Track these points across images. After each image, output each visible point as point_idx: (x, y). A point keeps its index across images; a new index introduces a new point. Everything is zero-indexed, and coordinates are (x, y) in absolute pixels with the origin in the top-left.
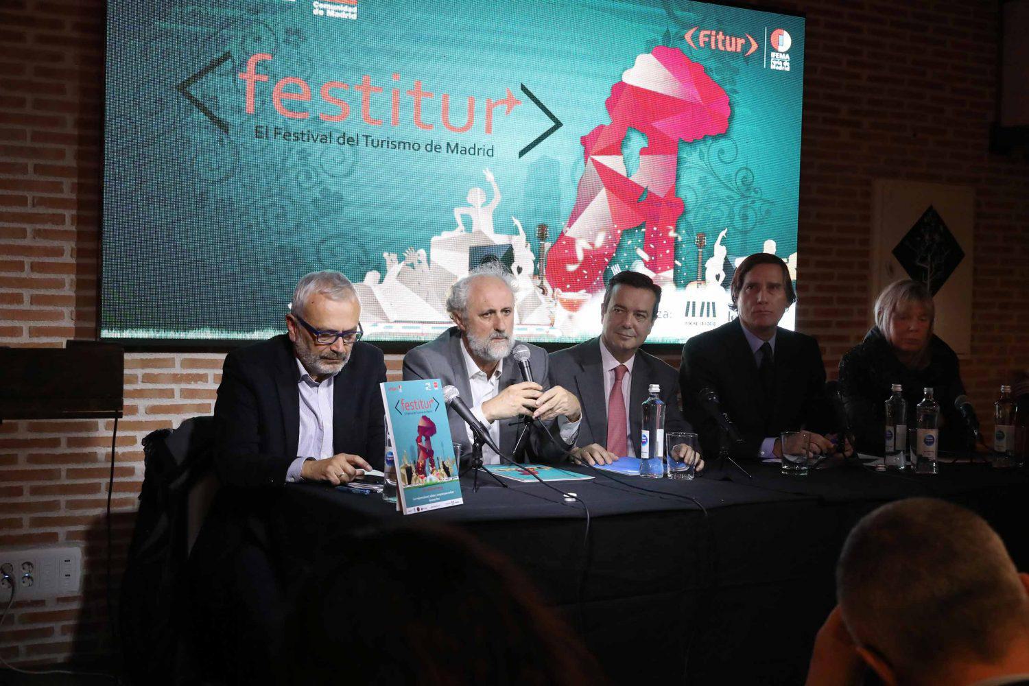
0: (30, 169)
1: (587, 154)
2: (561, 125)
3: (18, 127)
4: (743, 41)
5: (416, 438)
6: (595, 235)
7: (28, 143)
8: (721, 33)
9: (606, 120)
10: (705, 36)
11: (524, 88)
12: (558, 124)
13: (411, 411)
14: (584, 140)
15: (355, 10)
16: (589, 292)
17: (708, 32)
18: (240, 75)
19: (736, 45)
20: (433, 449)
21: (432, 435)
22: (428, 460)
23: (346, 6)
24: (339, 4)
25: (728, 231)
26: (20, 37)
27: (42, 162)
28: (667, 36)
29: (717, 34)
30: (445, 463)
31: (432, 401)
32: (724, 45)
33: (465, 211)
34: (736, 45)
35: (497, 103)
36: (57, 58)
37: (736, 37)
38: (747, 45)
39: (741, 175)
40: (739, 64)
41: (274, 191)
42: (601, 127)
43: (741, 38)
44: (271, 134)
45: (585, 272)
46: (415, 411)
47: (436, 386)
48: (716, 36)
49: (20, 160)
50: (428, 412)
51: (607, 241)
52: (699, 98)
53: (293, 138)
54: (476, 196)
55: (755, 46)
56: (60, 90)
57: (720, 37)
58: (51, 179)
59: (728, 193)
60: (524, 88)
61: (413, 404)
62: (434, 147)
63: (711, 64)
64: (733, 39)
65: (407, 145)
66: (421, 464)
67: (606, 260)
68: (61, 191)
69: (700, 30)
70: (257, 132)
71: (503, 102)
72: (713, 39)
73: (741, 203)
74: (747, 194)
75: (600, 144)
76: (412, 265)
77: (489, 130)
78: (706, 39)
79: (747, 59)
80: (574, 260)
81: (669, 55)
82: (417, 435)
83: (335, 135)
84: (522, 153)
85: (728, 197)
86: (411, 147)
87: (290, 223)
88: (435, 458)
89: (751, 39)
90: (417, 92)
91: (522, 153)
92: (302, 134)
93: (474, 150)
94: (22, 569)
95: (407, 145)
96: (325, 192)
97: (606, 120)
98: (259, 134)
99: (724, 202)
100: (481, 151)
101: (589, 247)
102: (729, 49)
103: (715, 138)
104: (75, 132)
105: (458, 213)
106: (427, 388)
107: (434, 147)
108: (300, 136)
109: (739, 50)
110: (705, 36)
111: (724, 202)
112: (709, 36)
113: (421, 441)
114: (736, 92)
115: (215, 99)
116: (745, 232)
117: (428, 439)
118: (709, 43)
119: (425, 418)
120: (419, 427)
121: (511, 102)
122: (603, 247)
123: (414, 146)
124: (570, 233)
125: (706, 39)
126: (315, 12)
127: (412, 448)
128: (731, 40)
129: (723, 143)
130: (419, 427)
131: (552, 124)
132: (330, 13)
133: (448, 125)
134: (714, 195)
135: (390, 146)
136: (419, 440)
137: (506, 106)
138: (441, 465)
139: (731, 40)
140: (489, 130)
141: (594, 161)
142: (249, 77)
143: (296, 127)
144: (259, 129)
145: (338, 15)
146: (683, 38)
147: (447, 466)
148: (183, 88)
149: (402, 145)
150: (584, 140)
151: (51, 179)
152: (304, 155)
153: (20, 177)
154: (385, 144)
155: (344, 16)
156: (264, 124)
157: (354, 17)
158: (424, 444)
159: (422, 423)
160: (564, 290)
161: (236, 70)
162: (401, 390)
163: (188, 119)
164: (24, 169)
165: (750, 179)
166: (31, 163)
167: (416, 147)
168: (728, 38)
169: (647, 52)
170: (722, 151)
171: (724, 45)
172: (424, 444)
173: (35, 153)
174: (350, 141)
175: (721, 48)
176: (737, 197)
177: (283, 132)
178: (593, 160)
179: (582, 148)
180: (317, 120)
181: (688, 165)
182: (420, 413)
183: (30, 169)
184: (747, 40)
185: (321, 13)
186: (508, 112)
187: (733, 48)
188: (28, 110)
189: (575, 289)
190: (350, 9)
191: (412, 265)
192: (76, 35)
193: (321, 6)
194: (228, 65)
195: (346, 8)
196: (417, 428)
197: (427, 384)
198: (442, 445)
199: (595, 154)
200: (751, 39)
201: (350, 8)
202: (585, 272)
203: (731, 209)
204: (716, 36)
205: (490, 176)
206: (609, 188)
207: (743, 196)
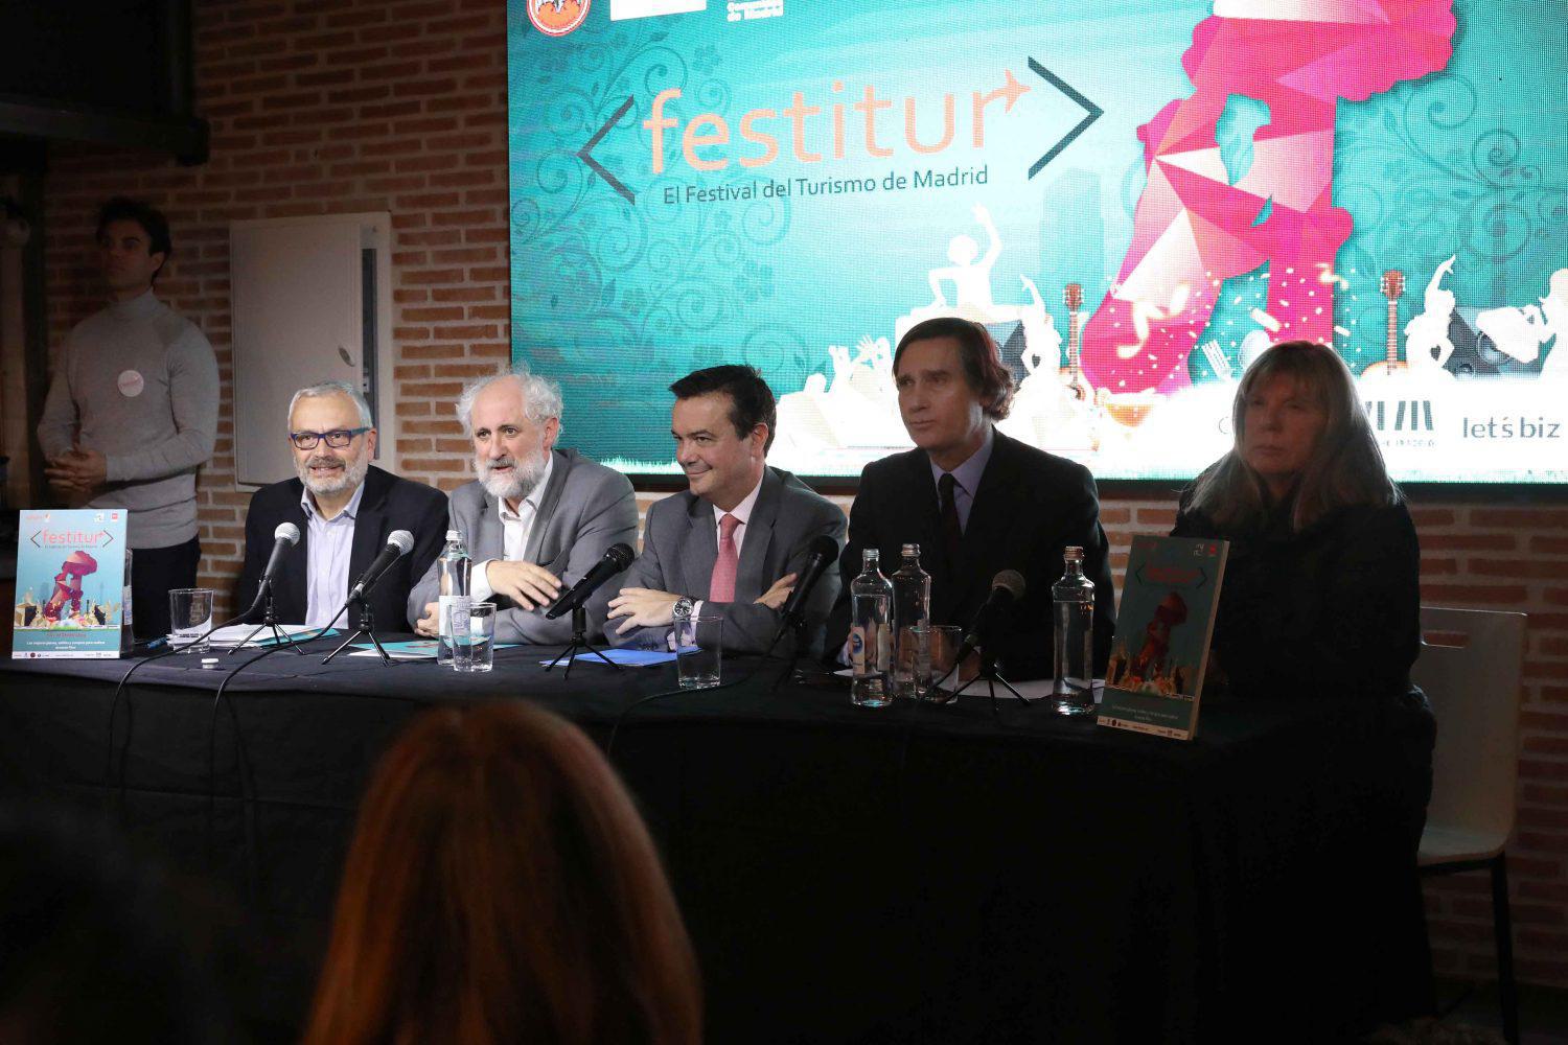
0: (467, 275)
1: (1149, 155)
7: (464, 245)
11: (1033, 64)
12: (1095, 112)
14: (1143, 133)
42: (1175, 105)
44: (683, 194)
53: (708, 197)
60: (1033, 64)
65: (857, 185)
73: (1491, 202)
84: (1033, 172)
86: (863, 186)
88: (83, 600)
91: (1033, 172)
103: (1420, 83)
108: (717, 194)
117: (77, 578)
127: (45, 587)
129: (1437, 91)
132: (747, 16)
135: (834, 189)
138: (92, 609)
149: (850, 185)
150: (1143, 133)
153: (457, 285)
154: (826, 187)
159: (72, 558)
162: (47, 520)
164: (459, 276)
166: (466, 267)
173: (469, 255)
177: (696, 191)
178: (1161, 164)
181: (1359, 143)
183: (467, 275)
186: (1008, 108)
188: (462, 207)
203: (1466, 218)
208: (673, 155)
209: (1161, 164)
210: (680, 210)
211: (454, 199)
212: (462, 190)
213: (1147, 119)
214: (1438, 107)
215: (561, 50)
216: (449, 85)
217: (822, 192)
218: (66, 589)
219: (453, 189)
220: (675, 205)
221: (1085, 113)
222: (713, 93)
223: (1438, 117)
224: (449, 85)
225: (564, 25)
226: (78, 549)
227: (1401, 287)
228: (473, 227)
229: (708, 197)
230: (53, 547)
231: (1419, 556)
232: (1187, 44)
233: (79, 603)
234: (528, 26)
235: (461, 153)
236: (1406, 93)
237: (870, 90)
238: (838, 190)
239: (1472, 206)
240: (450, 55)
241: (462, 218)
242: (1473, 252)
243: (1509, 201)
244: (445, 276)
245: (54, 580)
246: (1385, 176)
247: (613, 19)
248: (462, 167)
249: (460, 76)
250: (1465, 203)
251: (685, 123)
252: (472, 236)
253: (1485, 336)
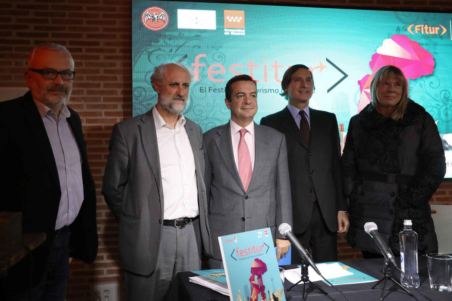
0: (103, 114)
1: (361, 89)
2: (348, 76)
3: (98, 96)
4: (438, 28)
5: (249, 278)
7: (102, 103)
8: (426, 26)
10: (418, 28)
11: (327, 60)
12: (346, 76)
13: (245, 257)
14: (359, 82)
15: (244, 31)
17: (420, 26)
19: (435, 31)
20: (264, 284)
21: (263, 273)
22: (260, 295)
23: (240, 30)
24: (236, 29)
25: (438, 121)
26: (98, 58)
27: (108, 110)
28: (398, 29)
29: (424, 26)
30: (275, 294)
31: (263, 246)
32: (429, 31)
34: (435, 31)
36: (113, 65)
37: (435, 27)
38: (441, 30)
39: (444, 92)
40: (438, 41)
41: (143, 103)
42: (368, 76)
43: (437, 27)
44: (207, 89)
46: (249, 255)
47: (266, 234)
48: (424, 28)
49: (99, 110)
50: (259, 255)
52: (418, 59)
53: (217, 91)
55: (445, 30)
56: (115, 78)
57: (426, 27)
58: (112, 118)
59: (436, 103)
60: (327, 60)
61: (247, 251)
63: (422, 41)
64: (433, 28)
65: (272, 91)
66: (254, 299)
69: (415, 24)
70: (201, 89)
71: (317, 67)
72: (422, 29)
73: (444, 107)
74: (447, 103)
78: (419, 29)
79: (441, 37)
81: (401, 40)
82: (251, 275)
84: (329, 91)
85: (437, 105)
86: (274, 91)
88: (266, 291)
89: (442, 27)
91: (329, 91)
92: (222, 89)
94: (105, 293)
95: (272, 91)
98: (202, 91)
99: (434, 107)
102: (431, 33)
103: (427, 76)
104: (122, 96)
106: (259, 237)
108: (221, 90)
109: (437, 33)
110: (418, 28)
111: (434, 107)
112: (420, 28)
113: (254, 280)
114: (436, 53)
116: (447, 122)
117: (260, 277)
118: (420, 31)
119: (257, 260)
120: (252, 269)
125: (419, 29)
126: (226, 33)
127: (246, 287)
128: (432, 29)
129: (431, 79)
130: (252, 269)
131: (343, 76)
132: (232, 34)
134: (429, 105)
135: (264, 91)
136: (252, 279)
137: (319, 69)
138: (272, 297)
139: (432, 29)
144: (202, 88)
145: (236, 34)
146: (406, 30)
147: (277, 296)
149: (270, 90)
150: (359, 82)
151: (112, 118)
153: (99, 118)
154: (262, 91)
155: (239, 34)
156: (204, 86)
157: (244, 34)
158: (256, 282)
159: (255, 265)
162: (236, 241)
164: (100, 114)
165: (448, 95)
166: (103, 111)
167: (277, 91)
168: (430, 28)
169: (388, 38)
170: (431, 83)
171: (429, 31)
172: (256, 282)
173: (104, 106)
175: (427, 33)
176: (441, 104)
177: (213, 89)
178: (364, 91)
179: (359, 86)
181: (414, 90)
182: (253, 257)
183: (103, 114)
184: (441, 28)
185: (228, 34)
186: (320, 72)
187: (433, 32)
188: (102, 88)
190: (242, 31)
192: (121, 54)
193: (228, 30)
195: (240, 30)
196: (250, 270)
197: (258, 233)
198: (272, 280)
199: (365, 89)
200: (442, 27)
201: (242, 30)
203: (439, 110)
204: (424, 28)
206: (255, 287)
207: (445, 104)
208: (203, 76)
209: (364, 91)
210: (206, 95)
211: (98, 85)
212: (102, 83)
213: (360, 79)
214: (431, 83)
215: (157, 36)
216: (97, 44)
217: (260, 92)
218: (256, 286)
219: (97, 82)
220: (205, 93)
221: (343, 76)
222: (219, 57)
223: (432, 85)
224: (97, 44)
225: (159, 27)
226: (256, 258)
227: (343, 128)
228: (106, 96)
229: (217, 91)
230: (243, 259)
231: (96, 205)
232: (370, 60)
233: (265, 294)
234: (141, 25)
235: (102, 69)
236: (424, 78)
237: (276, 62)
238: (266, 92)
239: (440, 108)
240: (97, 33)
241: (102, 92)
242: (441, 120)
243: (448, 107)
244: (93, 114)
245: (249, 282)
246: (421, 99)
247: (178, 28)
248: (101, 74)
249: (102, 41)
250: (439, 107)
251: (208, 66)
252: (105, 100)
253: (445, 141)
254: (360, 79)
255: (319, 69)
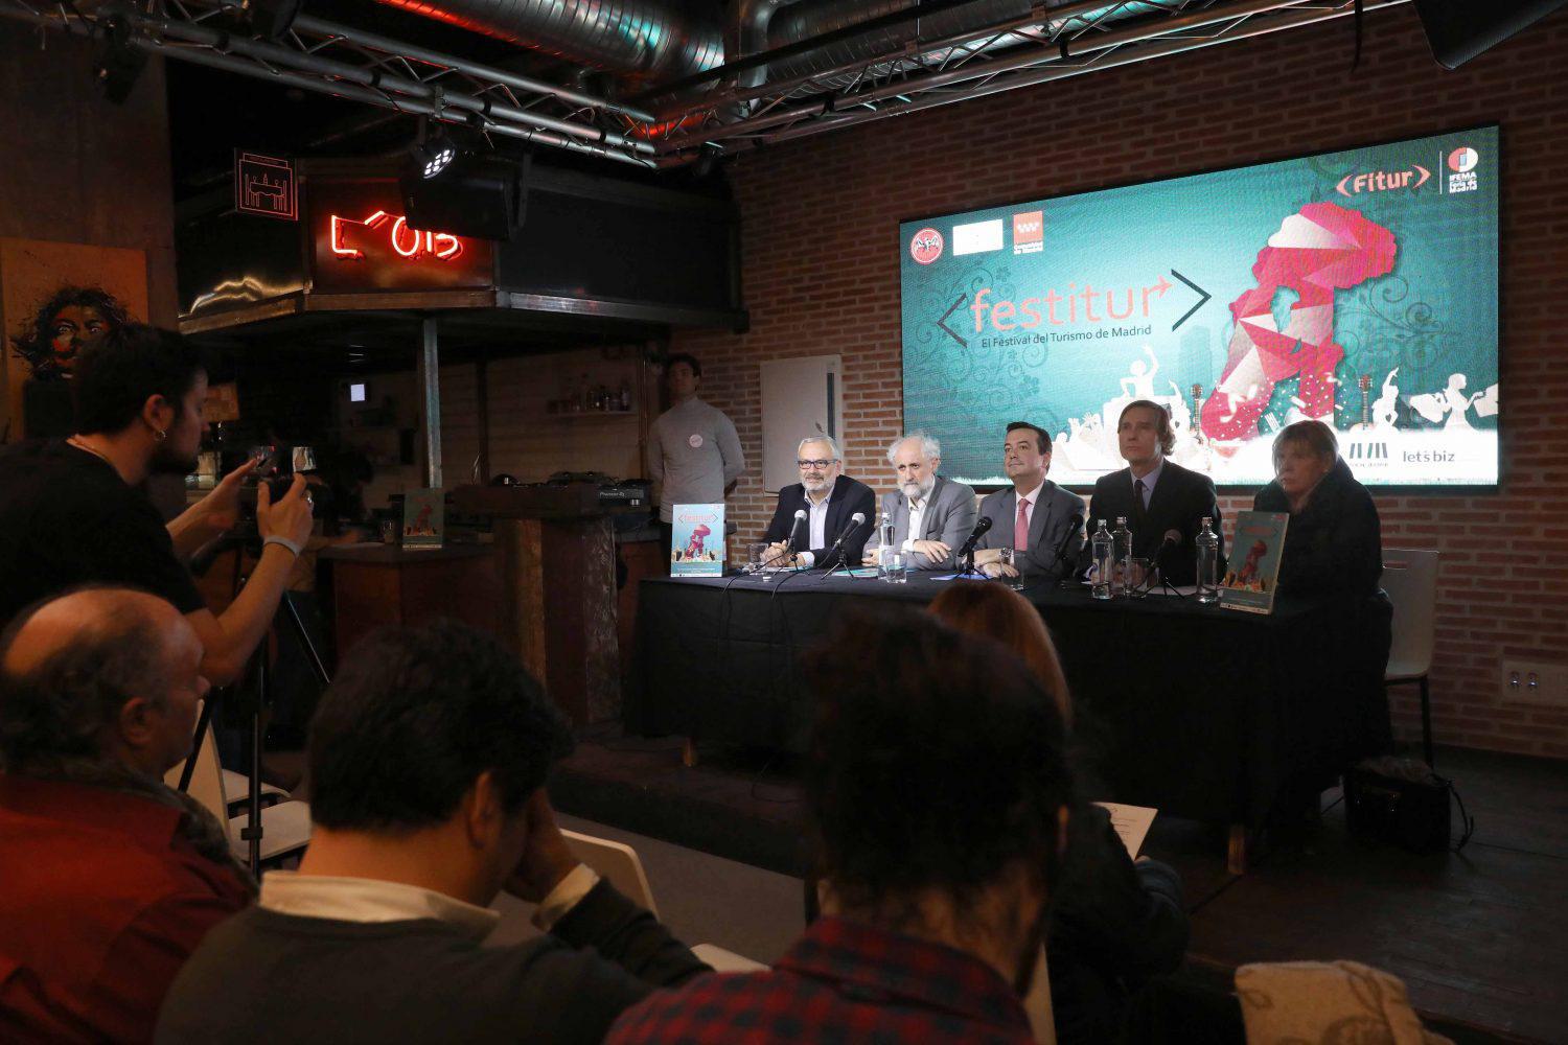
1: (1235, 317)
6: (1247, 389)
9: (1253, 285)
11: (1174, 273)
12: (1207, 297)
14: (1232, 307)
16: (1245, 439)
18: (972, 307)
33: (1130, 380)
35: (1151, 291)
42: (1249, 292)
45: (1239, 422)
51: (1259, 392)
54: (1137, 367)
60: (1174, 273)
62: (1102, 334)
67: (1260, 410)
68: (894, 396)
71: (1155, 288)
75: (1250, 305)
76: (1090, 427)
77: (1146, 313)
80: (1227, 412)
83: (1032, 337)
84: (1175, 327)
87: (1006, 402)
90: (1088, 295)
91: (1175, 327)
93: (1134, 331)
96: (1027, 379)
97: (1253, 285)
100: (1140, 331)
101: (1241, 400)
105: (1123, 382)
107: (1102, 334)
115: (958, 326)
121: (1164, 287)
122: (1255, 399)
123: (1088, 336)
124: (1222, 389)
133: (1113, 316)
140: (1146, 313)
141: (1242, 323)
142: (978, 308)
143: (1007, 336)
148: (941, 324)
152: (1013, 355)
160: (1219, 439)
161: (969, 303)
163: (945, 342)
174: (1041, 339)
180: (1020, 329)
189: (1229, 437)
191: (1090, 427)
194: (965, 302)
202: (1239, 422)
205: (1149, 350)
232: (1254, 260)
254: (1234, 298)
255: (1158, 292)
